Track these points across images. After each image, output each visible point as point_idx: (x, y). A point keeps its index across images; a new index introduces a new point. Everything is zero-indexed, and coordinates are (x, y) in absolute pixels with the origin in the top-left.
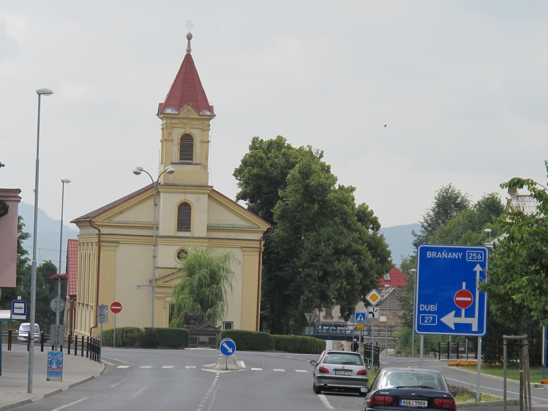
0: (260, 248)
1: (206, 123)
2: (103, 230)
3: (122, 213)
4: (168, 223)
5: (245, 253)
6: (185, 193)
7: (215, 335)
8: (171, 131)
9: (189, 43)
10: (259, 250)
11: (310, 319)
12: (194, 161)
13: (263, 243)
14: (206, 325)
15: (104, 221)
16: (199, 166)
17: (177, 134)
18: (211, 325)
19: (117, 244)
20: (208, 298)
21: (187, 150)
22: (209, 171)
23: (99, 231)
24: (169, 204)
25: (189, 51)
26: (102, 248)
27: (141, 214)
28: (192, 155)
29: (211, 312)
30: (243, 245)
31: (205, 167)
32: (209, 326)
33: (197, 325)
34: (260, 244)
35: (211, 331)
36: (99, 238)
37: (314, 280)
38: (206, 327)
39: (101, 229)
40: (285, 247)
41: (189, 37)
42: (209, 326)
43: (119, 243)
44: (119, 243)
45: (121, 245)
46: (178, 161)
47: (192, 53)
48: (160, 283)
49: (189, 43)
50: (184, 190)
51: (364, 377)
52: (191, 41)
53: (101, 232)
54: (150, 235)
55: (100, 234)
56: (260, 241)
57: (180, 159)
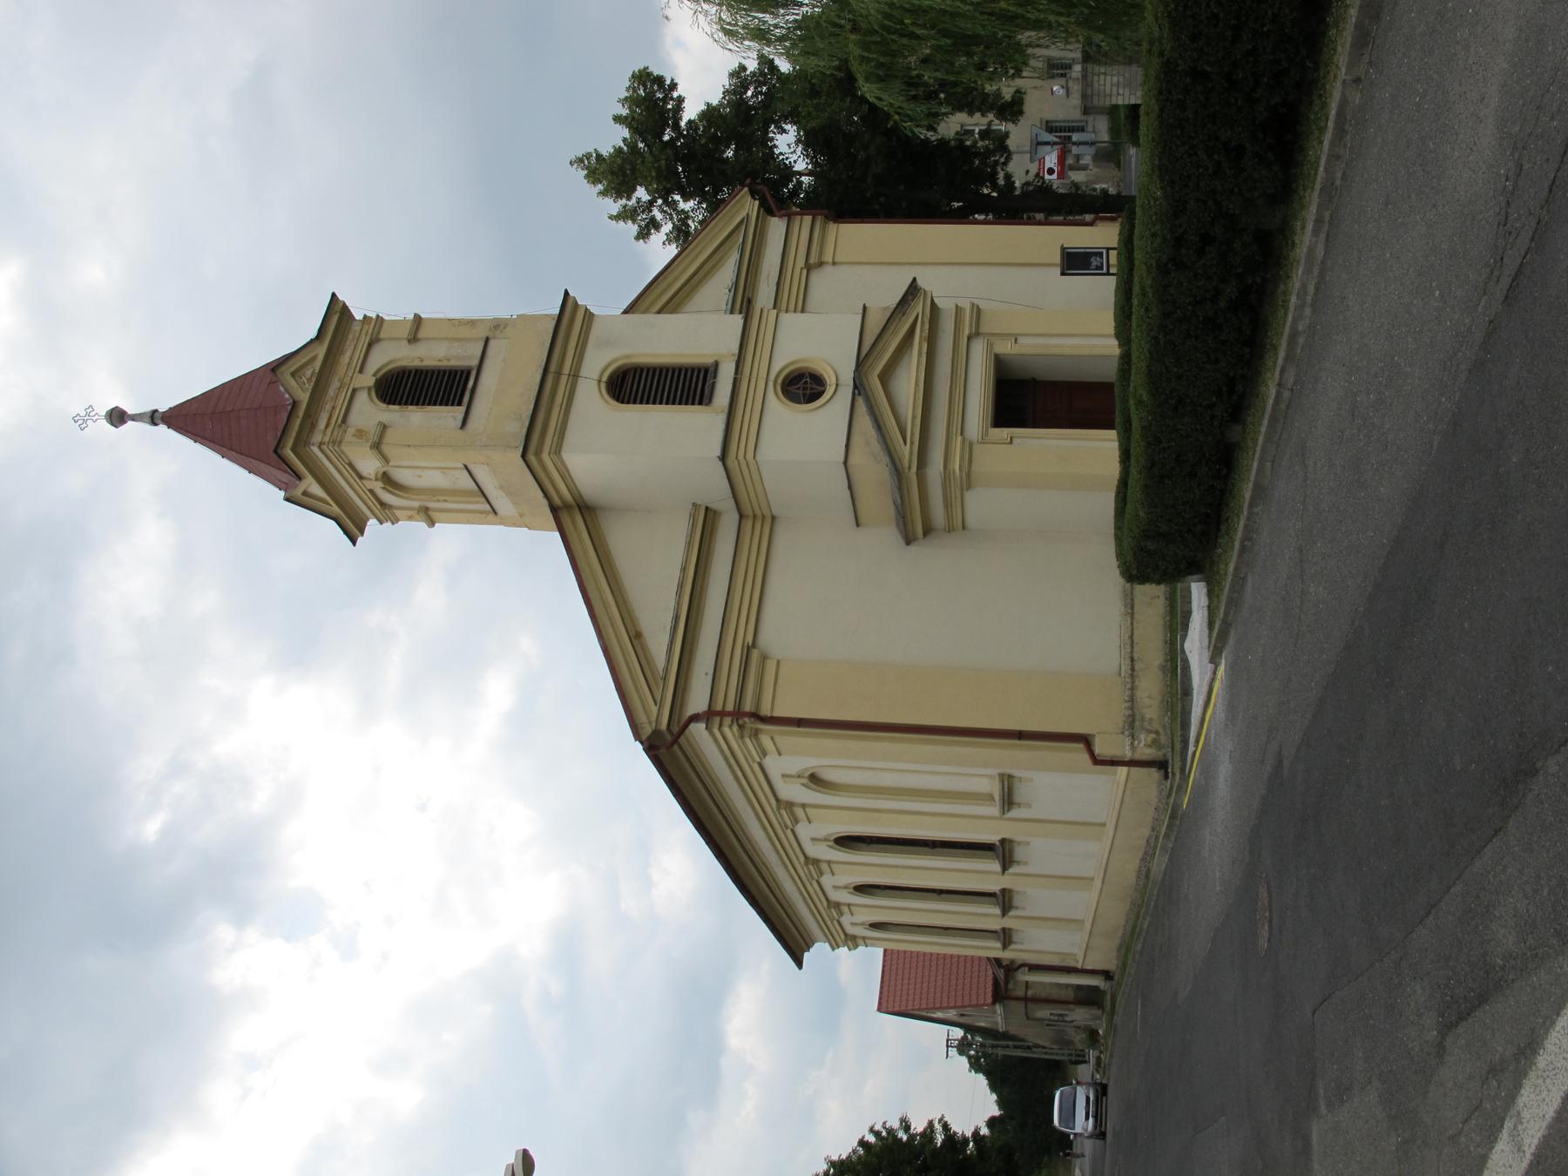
1: (356, 328)
2: (698, 701)
4: (687, 433)
5: (828, 257)
6: (575, 376)
8: (351, 431)
9: (134, 418)
15: (658, 698)
16: (492, 343)
19: (755, 654)
21: (434, 386)
23: (695, 718)
24: (613, 447)
25: (153, 418)
26: (765, 711)
27: (653, 567)
30: (801, 262)
36: (723, 714)
41: (117, 417)
43: (748, 650)
45: (768, 638)
47: (163, 408)
48: (907, 452)
49: (134, 418)
50: (564, 379)
52: (130, 411)
54: (731, 525)
55: (708, 716)
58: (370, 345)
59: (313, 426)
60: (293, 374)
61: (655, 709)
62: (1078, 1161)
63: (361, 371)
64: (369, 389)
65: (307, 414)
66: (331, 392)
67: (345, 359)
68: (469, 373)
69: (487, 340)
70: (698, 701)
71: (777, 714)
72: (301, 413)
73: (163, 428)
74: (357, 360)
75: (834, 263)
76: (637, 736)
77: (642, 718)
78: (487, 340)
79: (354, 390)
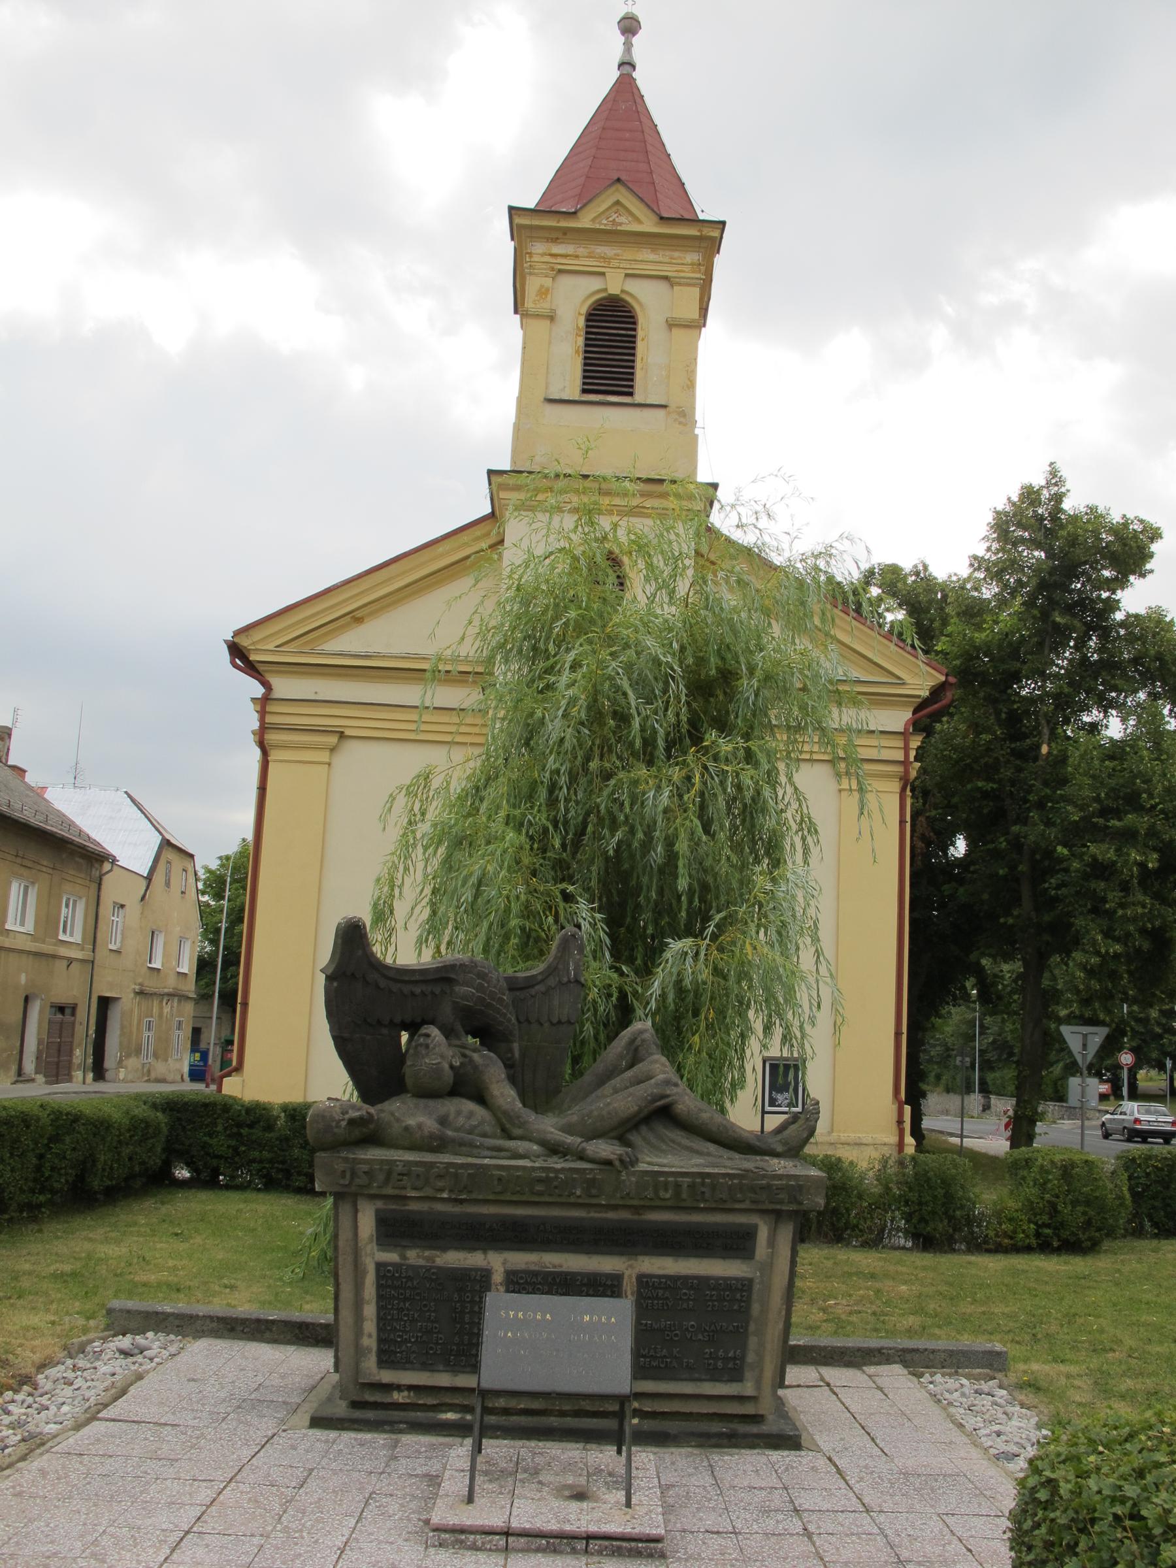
0: (905, 763)
3: (359, 620)
7: (737, 1243)
9: (628, 46)
10: (901, 769)
11: (1085, 1046)
12: (638, 398)
13: (916, 742)
14: (620, 1100)
16: (660, 413)
17: (573, 299)
18: (687, 1102)
20: (672, 857)
21: (609, 353)
22: (697, 431)
25: (627, 64)
26: (274, 755)
28: (630, 377)
29: (698, 972)
31: (684, 416)
32: (662, 1114)
33: (505, 1094)
34: (906, 749)
35: (700, 1190)
37: (1125, 888)
38: (624, 1130)
39: (277, 682)
40: (980, 784)
41: (629, 26)
42: (662, 1114)
44: (342, 735)
45: (351, 747)
46: (576, 395)
47: (640, 76)
49: (628, 46)
51: (781, 1069)
52: (635, 40)
53: (277, 694)
56: (904, 735)
57: (584, 391)
58: (666, 278)
59: (555, 240)
60: (618, 203)
61: (271, 647)
62: (482, 1256)
63: (627, 275)
64: (605, 290)
65: (566, 231)
66: (600, 250)
67: (647, 255)
68: (631, 394)
69: (664, 407)
70: (284, 687)
71: (271, 765)
72: (564, 224)
73: (616, 74)
74: (640, 268)
75: (840, 791)
76: (237, 633)
77: (257, 635)
78: (664, 407)
79: (603, 274)
